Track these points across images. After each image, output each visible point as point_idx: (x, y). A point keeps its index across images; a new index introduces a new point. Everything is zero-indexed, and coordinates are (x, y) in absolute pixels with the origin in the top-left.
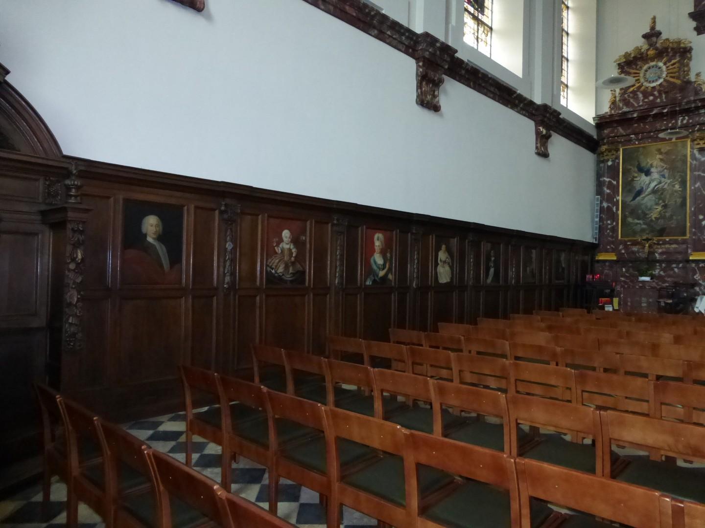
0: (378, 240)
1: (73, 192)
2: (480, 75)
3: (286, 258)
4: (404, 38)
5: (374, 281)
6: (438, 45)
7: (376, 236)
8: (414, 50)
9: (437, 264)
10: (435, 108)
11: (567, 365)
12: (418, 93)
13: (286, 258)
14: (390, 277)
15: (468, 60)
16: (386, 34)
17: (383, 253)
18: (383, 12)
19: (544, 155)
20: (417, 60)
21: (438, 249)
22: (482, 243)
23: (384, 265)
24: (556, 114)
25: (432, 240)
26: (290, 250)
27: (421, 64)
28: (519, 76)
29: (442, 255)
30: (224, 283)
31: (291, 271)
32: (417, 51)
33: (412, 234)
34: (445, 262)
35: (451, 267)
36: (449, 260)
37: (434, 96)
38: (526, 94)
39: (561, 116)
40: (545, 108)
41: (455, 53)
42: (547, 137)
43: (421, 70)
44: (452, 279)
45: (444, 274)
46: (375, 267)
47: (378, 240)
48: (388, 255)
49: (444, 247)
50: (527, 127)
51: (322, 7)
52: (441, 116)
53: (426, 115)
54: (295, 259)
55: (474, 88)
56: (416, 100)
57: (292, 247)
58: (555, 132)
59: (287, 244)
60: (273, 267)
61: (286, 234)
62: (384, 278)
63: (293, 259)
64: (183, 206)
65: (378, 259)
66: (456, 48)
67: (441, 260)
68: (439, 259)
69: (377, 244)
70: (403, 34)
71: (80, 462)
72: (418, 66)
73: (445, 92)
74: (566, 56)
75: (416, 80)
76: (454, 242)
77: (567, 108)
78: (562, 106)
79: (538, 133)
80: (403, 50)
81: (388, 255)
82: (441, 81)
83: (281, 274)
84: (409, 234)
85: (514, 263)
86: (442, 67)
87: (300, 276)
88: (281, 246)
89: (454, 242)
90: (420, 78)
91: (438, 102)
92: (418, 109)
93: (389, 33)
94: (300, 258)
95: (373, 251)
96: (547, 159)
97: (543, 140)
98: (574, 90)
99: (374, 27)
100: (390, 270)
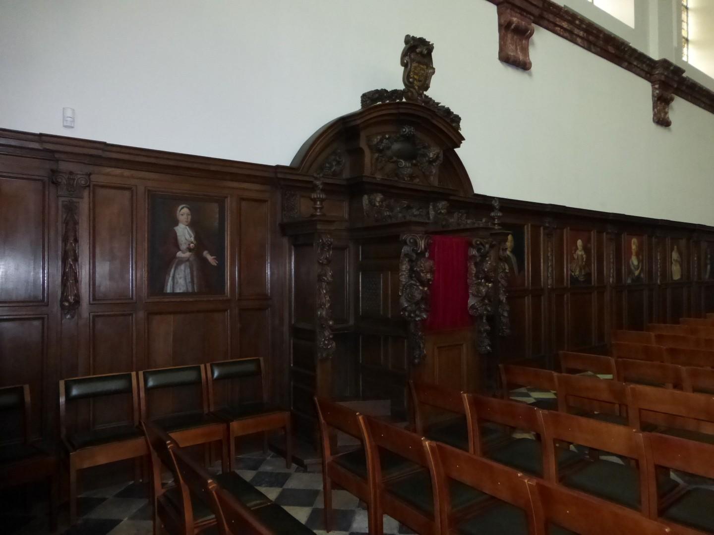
0: (634, 243)
1: (496, 221)
2: (697, 89)
3: (580, 263)
4: (644, 65)
5: (633, 280)
6: (672, 68)
7: (633, 241)
8: (651, 75)
9: (672, 263)
10: (524, 66)
11: (696, 390)
12: (655, 112)
13: (580, 263)
14: (642, 275)
15: (564, 5)
16: (633, 64)
17: (637, 255)
18: (631, 45)
19: (662, 121)
20: (653, 83)
21: (672, 250)
22: (623, 236)
23: (638, 265)
24: (678, 71)
25: (566, 232)
26: (582, 256)
27: (657, 86)
28: (629, 25)
29: (675, 255)
30: (548, 285)
31: (583, 273)
32: (653, 75)
33: (607, 233)
34: (676, 261)
35: (681, 266)
36: (679, 259)
37: (666, 113)
38: (640, 48)
39: (684, 75)
40: (665, 64)
41: (683, 73)
42: (524, 34)
43: (657, 92)
44: (682, 275)
45: (676, 272)
46: (633, 268)
47: (634, 243)
48: (641, 257)
49: (675, 247)
50: (642, 90)
51: (593, 50)
52: (530, 75)
53: (660, 130)
54: (585, 264)
55: (691, 101)
56: (653, 118)
57: (583, 253)
58: (677, 94)
59: (580, 251)
60: (573, 270)
61: (579, 243)
62: (638, 277)
63: (584, 263)
64: (523, 226)
65: (634, 261)
66: (684, 69)
67: (674, 260)
68: (673, 258)
69: (634, 247)
70: (644, 62)
71: (195, 517)
72: (654, 89)
73: (533, 44)
74: (685, 4)
75: (653, 101)
76: (683, 242)
77: (687, 62)
78: (684, 61)
79: (505, 28)
80: (586, 46)
81: (641, 257)
82: (672, 99)
83: (577, 276)
84: (605, 234)
85: (659, 258)
86: (672, 86)
87: (588, 275)
88: (577, 253)
89: (683, 242)
90: (656, 99)
91: (668, 118)
92: (653, 126)
93: (635, 63)
94: (588, 263)
95: (631, 254)
96: (667, 128)
97: (662, 102)
98: (696, 43)
99: (626, 61)
100: (642, 269)
